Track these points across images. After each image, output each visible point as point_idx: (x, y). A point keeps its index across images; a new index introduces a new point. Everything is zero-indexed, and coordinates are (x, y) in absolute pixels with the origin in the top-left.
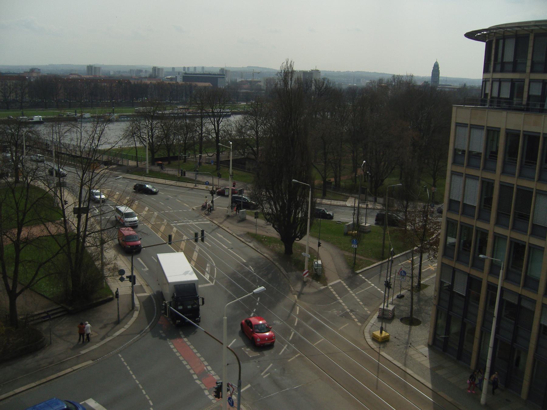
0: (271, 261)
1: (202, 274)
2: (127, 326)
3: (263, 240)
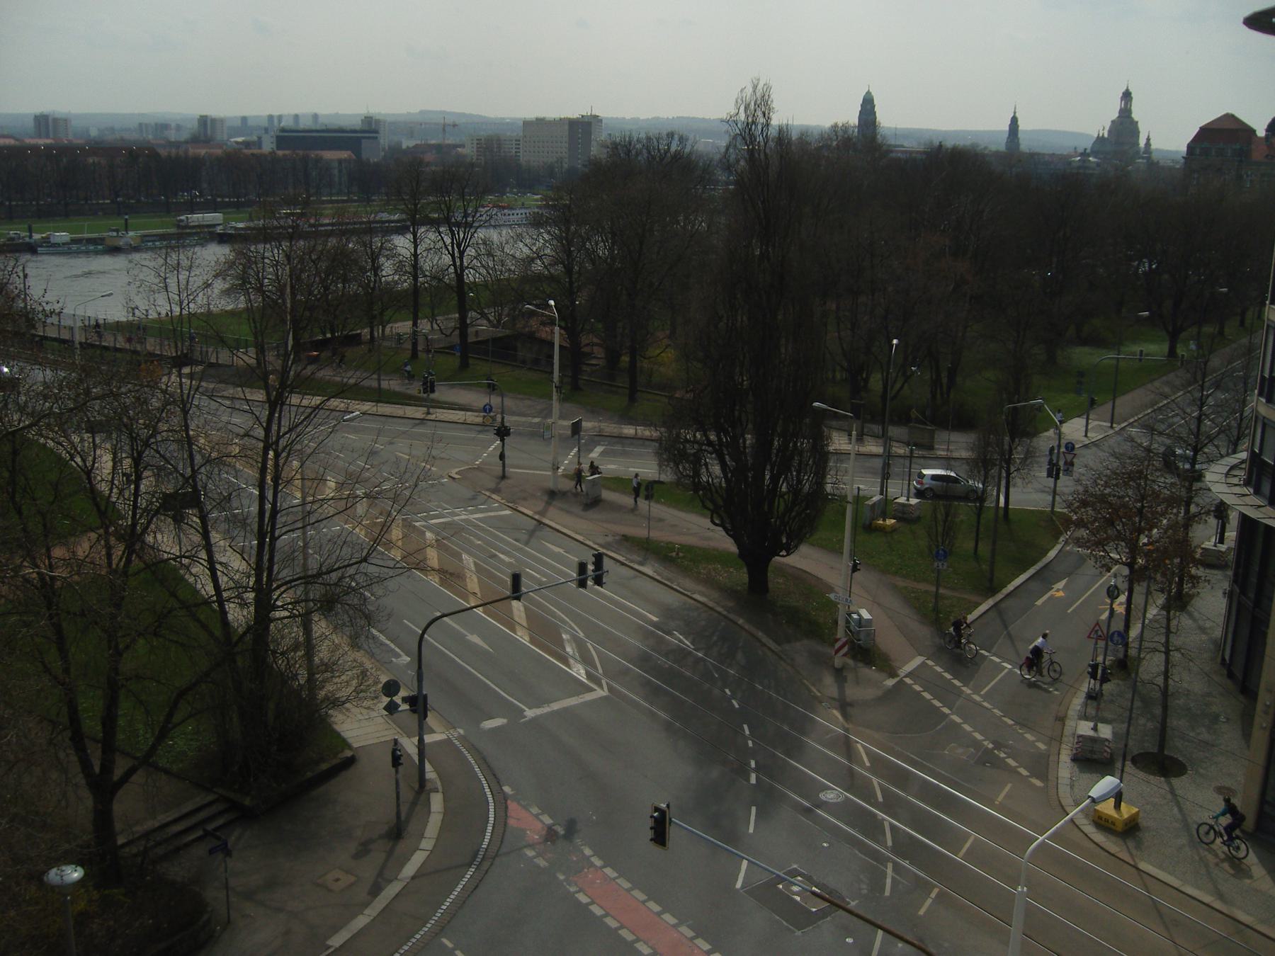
0: (719, 613)
1: (564, 667)
2: (427, 844)
3: (674, 554)
